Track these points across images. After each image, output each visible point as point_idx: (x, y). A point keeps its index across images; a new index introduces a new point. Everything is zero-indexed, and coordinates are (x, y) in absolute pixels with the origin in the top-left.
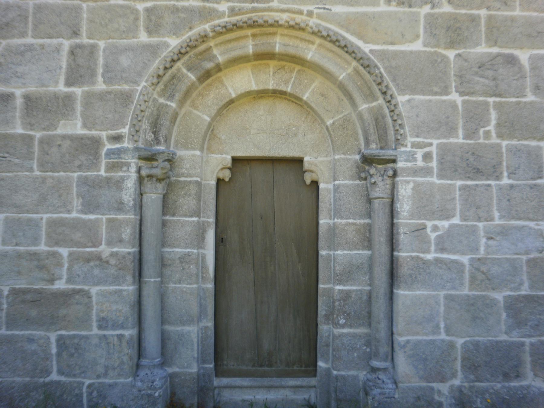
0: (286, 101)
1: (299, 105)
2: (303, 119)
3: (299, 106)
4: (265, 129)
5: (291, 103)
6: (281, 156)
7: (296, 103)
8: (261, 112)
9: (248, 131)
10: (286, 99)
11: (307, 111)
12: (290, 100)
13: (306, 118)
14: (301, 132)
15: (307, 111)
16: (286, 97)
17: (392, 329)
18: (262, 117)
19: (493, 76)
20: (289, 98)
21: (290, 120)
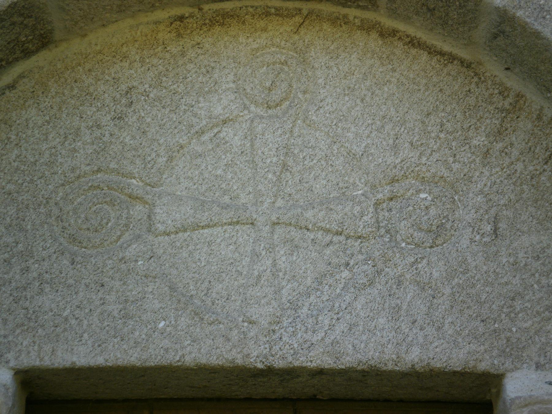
0: (374, 42)
1: (452, 58)
2: (479, 140)
3: (453, 68)
4: (244, 199)
5: (399, 48)
6: (348, 360)
7: (432, 51)
8: (221, 105)
9: (138, 211)
10: (367, 27)
11: (504, 92)
12: (394, 33)
13: (500, 133)
14: (470, 217)
15: (504, 92)
16: (369, 15)
17: (240, 400)
18: (227, 132)
19: (487, 136)
20: (389, 23)
21: (395, 148)
